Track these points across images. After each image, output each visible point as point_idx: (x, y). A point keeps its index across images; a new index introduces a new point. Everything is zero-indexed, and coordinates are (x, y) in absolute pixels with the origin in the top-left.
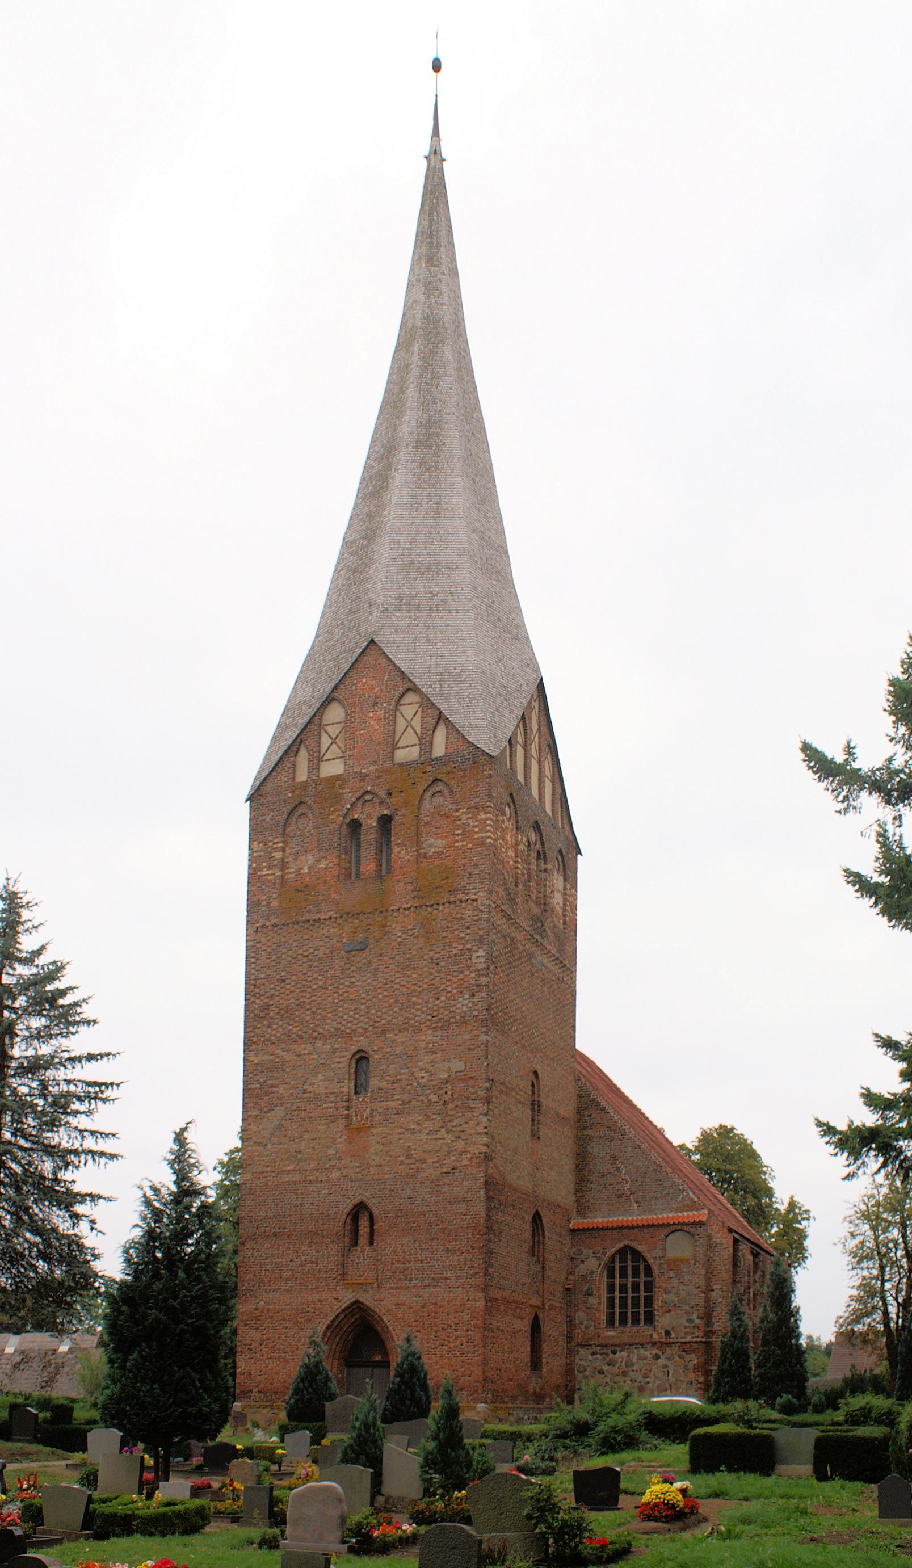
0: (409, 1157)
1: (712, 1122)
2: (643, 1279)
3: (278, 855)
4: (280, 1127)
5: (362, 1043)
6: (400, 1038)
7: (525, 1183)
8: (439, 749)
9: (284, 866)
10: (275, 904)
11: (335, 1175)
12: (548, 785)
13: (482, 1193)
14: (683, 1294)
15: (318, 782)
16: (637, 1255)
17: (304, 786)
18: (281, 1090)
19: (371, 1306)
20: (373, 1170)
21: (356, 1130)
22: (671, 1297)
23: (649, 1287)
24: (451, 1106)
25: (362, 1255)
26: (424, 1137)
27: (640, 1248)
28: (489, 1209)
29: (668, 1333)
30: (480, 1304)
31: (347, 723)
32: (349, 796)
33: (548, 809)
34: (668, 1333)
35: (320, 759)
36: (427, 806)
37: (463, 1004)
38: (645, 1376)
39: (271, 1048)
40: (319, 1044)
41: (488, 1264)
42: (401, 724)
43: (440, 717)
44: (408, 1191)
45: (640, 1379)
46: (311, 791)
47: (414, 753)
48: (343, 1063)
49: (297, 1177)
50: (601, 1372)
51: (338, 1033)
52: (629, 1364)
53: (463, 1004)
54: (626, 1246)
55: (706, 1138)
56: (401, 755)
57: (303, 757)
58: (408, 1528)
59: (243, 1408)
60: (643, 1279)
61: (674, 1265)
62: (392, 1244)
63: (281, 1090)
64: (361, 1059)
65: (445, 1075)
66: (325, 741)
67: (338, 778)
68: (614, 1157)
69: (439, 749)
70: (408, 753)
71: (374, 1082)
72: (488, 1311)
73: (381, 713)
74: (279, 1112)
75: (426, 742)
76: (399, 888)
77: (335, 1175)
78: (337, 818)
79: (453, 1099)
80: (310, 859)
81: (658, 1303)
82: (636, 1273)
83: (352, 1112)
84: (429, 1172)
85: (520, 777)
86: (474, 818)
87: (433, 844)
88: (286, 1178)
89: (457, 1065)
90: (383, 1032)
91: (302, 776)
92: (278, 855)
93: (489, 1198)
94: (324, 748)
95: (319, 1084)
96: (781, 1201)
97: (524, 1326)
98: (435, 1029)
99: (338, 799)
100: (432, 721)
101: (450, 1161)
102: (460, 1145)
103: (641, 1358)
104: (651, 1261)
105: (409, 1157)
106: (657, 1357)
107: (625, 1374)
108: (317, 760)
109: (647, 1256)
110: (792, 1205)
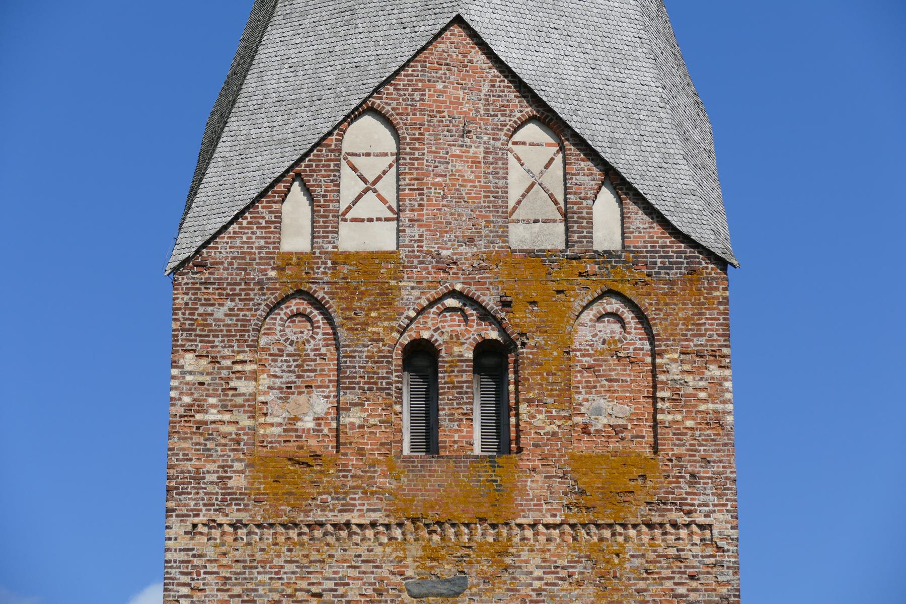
15: (341, 259)
56: (521, 236)
57: (296, 208)
66: (350, 185)
67: (384, 256)
75: (573, 217)
76: (535, 485)
91: (296, 237)
99: (386, 297)
108: (326, 216)
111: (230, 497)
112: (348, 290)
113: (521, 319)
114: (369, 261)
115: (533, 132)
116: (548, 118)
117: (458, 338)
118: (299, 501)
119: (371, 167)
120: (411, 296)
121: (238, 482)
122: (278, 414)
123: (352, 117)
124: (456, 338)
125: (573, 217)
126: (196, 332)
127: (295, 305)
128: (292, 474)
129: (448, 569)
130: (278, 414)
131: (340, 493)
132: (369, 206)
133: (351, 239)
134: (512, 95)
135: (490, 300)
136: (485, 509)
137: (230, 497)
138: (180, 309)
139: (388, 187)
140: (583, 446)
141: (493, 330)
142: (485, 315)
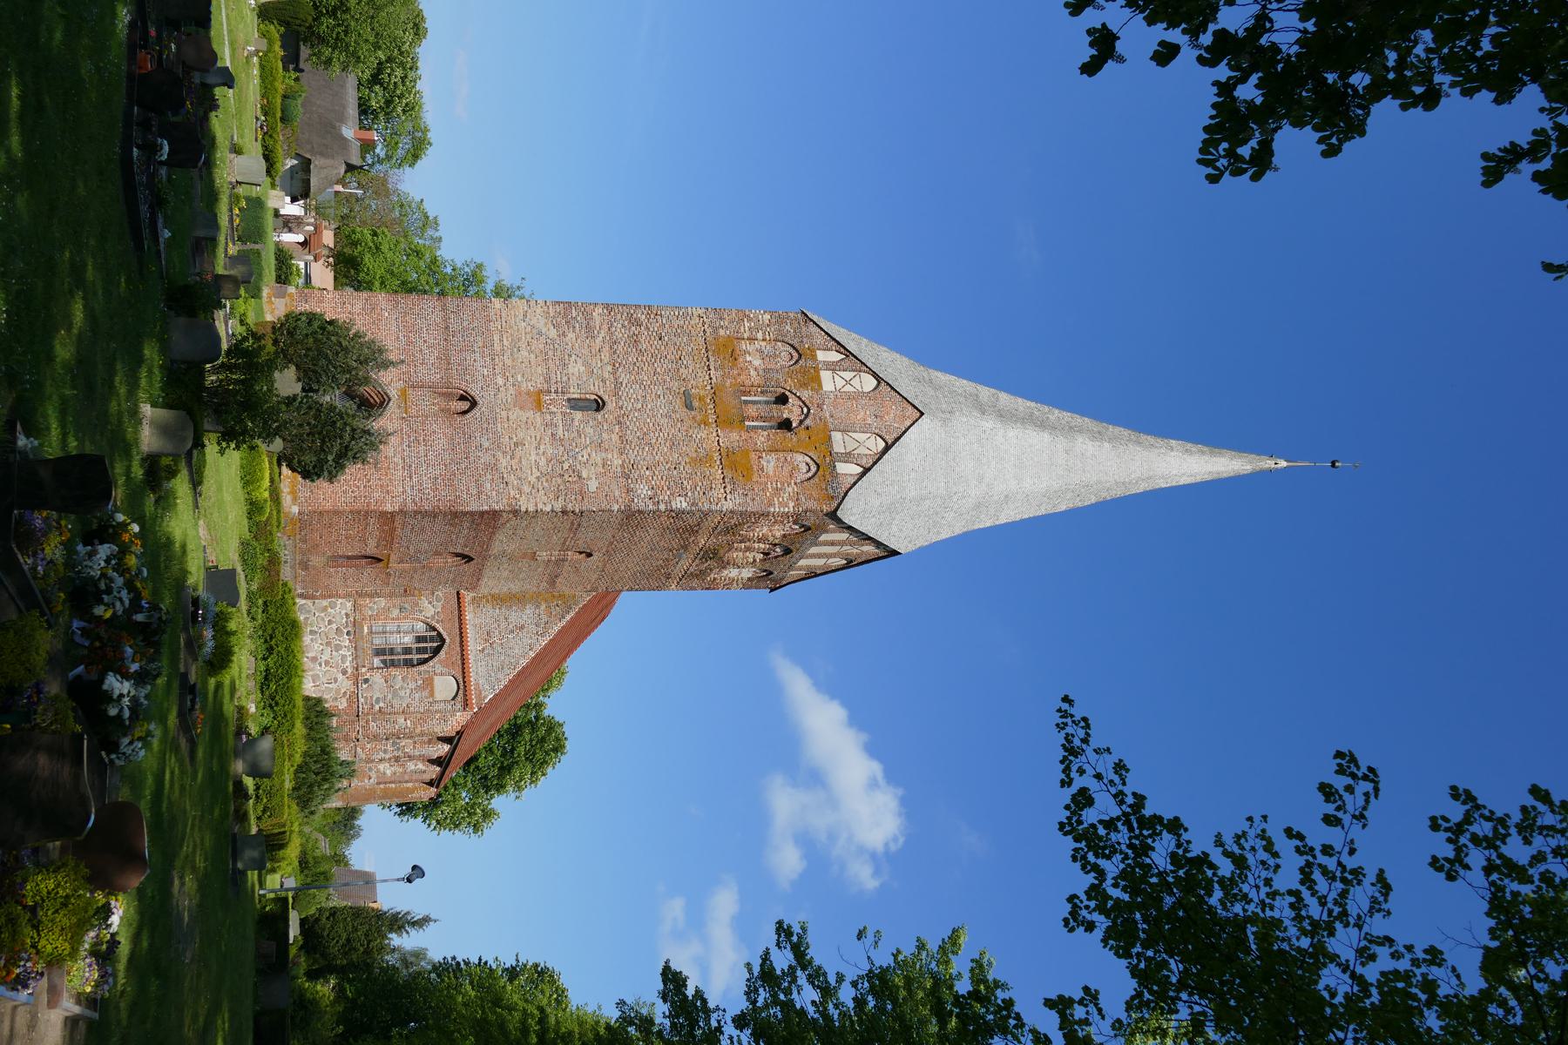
0: (516, 444)
1: (572, 734)
2: (415, 657)
3: (760, 335)
4: (540, 333)
5: (610, 406)
6: (615, 437)
7: (496, 548)
8: (842, 468)
9: (752, 339)
10: (722, 332)
11: (500, 381)
12: (820, 562)
13: (486, 508)
14: (402, 693)
15: (817, 370)
16: (437, 651)
17: (814, 357)
18: (571, 335)
19: (342, 317)
20: (504, 414)
21: (537, 401)
22: (399, 683)
23: (409, 664)
24: (560, 481)
25: (425, 403)
26: (533, 458)
27: (442, 653)
28: (472, 514)
29: (366, 681)
30: (389, 508)
31: (859, 395)
32: (805, 394)
33: (802, 562)
34: (366, 681)
35: (834, 370)
36: (800, 458)
37: (643, 490)
38: (327, 663)
39: (605, 327)
40: (609, 368)
41: (425, 514)
42: (861, 437)
43: (867, 470)
44: (486, 444)
45: (324, 658)
46: (810, 363)
47: (838, 448)
48: (594, 388)
49: (497, 347)
50: (330, 622)
51: (618, 384)
52: (338, 648)
53: (643, 490)
54: (443, 641)
55: (552, 726)
56: (837, 436)
57: (835, 356)
58: (280, 88)
59: (291, 295)
60: (415, 657)
61: (428, 684)
62: (440, 433)
63: (571, 335)
64: (599, 405)
65: (584, 475)
66: (848, 375)
67: (820, 386)
68: (522, 627)
69: (842, 468)
70: (839, 442)
71: (578, 415)
72: (383, 514)
73: (869, 421)
74: (553, 333)
75: (848, 457)
76: (734, 436)
77: (500, 381)
78: (790, 384)
79: (565, 482)
80: (757, 362)
81: (393, 671)
82: (419, 651)
83: (553, 396)
84: (504, 462)
85: (823, 537)
86: (790, 498)
87: (770, 463)
88: (496, 338)
89: (593, 485)
90: (619, 423)
91: (821, 356)
92: (760, 335)
93: (482, 514)
94: (842, 374)
95: (576, 368)
96: (498, 802)
97: (371, 549)
98: (622, 466)
99: (804, 385)
100: (864, 462)
101: (512, 479)
102: (526, 489)
103: (344, 657)
104: (431, 663)
105: (516, 444)
106: (344, 672)
107: (328, 644)
108: (833, 367)
109: (436, 659)
110: (488, 815)
111: (716, 330)
112: (804, 371)
113: (803, 434)
114: (817, 380)
115: (882, 445)
116: (887, 448)
117: (792, 411)
118: (717, 352)
119: (856, 382)
120: (805, 394)
121: (722, 332)
122: (750, 348)
123: (875, 375)
124: (791, 411)
125: (848, 457)
126: (780, 320)
127: (795, 355)
128: (728, 351)
129: (696, 404)
130: (750, 348)
131: (722, 367)
132: (840, 383)
133: (825, 375)
134: (895, 435)
135: (808, 422)
136: (722, 418)
137: (716, 330)
138: (430, 569)
139: (848, 388)
140: (753, 456)
141: (134, 779)
142: (801, 422)
